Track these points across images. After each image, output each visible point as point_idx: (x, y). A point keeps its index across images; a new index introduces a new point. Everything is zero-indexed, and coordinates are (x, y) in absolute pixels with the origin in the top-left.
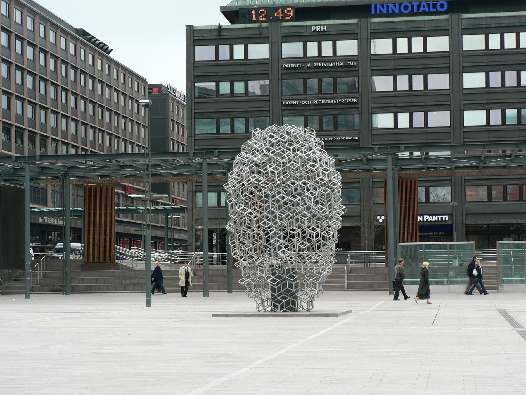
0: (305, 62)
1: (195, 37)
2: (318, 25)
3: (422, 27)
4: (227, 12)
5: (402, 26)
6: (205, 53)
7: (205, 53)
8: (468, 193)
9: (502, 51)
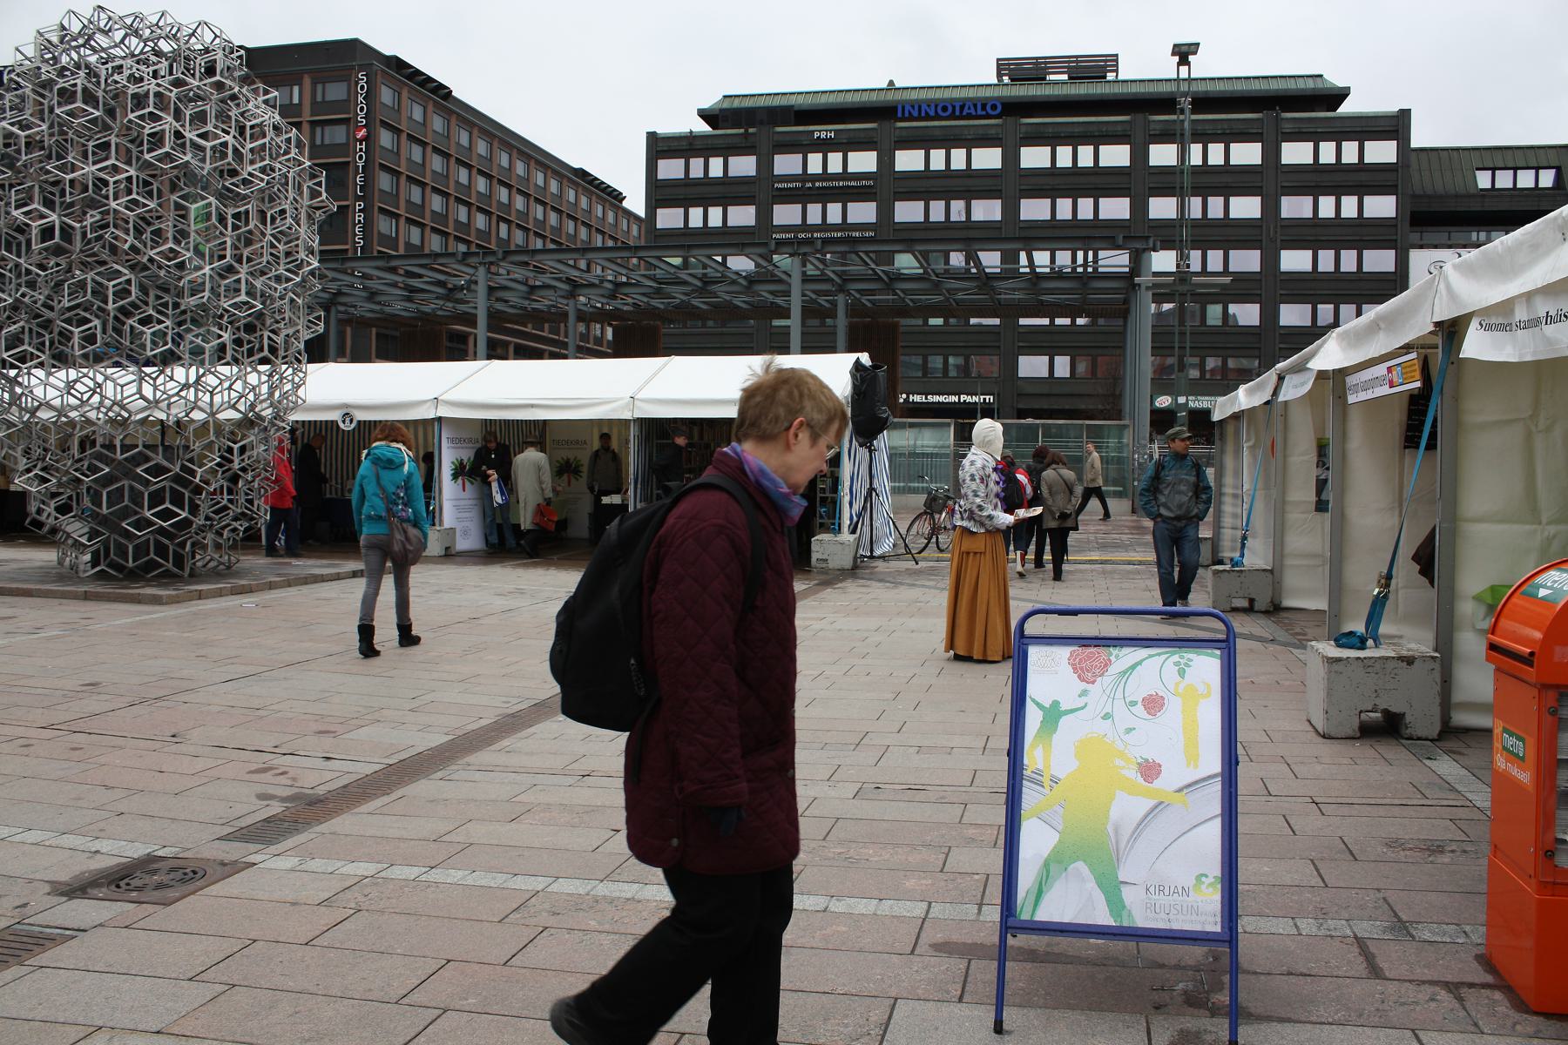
0: (804, 181)
1: (659, 147)
2: (823, 132)
3: (1306, 128)
4: (705, 115)
5: (937, 133)
6: (671, 169)
7: (671, 169)
8: (995, 369)
9: (948, 173)
